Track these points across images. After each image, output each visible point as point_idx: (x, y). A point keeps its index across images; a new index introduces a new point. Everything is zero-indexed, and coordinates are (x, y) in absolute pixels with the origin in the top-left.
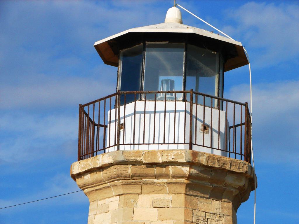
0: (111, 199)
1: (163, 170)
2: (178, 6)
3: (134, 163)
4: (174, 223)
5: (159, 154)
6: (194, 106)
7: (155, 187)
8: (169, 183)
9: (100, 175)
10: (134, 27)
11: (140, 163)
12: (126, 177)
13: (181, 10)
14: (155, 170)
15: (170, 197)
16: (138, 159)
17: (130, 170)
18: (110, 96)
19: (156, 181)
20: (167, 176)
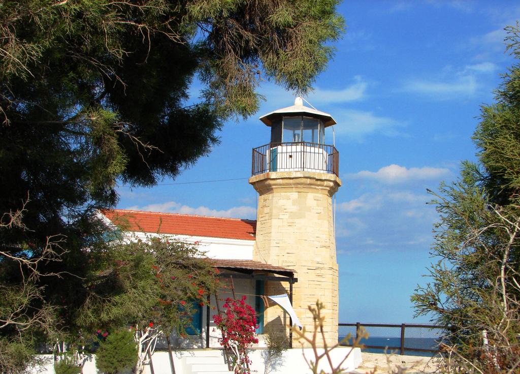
0: (292, 193)
1: (322, 183)
2: (514, 281)
3: (310, 178)
4: (59, 361)
5: (323, 175)
6: (305, 147)
7: (315, 190)
8: (322, 189)
9: (291, 181)
10: (273, 111)
11: (314, 178)
12: (306, 184)
13: (303, 100)
14: (319, 183)
15: (321, 195)
16: (315, 177)
17: (308, 181)
18: (266, 145)
19: (317, 187)
20: (322, 186)
